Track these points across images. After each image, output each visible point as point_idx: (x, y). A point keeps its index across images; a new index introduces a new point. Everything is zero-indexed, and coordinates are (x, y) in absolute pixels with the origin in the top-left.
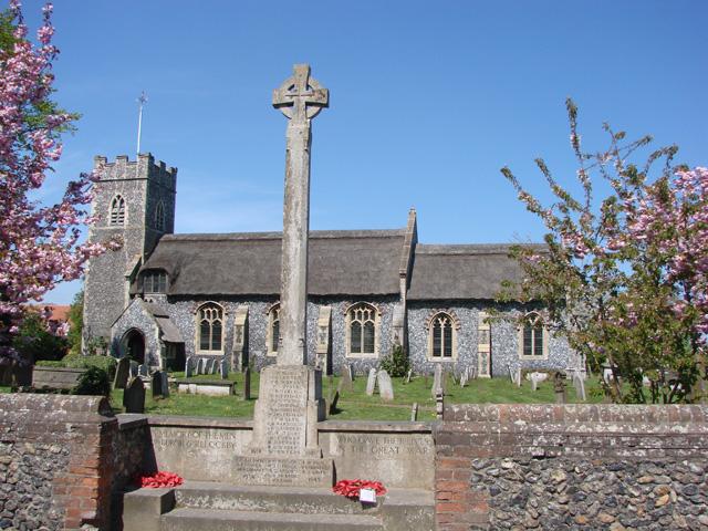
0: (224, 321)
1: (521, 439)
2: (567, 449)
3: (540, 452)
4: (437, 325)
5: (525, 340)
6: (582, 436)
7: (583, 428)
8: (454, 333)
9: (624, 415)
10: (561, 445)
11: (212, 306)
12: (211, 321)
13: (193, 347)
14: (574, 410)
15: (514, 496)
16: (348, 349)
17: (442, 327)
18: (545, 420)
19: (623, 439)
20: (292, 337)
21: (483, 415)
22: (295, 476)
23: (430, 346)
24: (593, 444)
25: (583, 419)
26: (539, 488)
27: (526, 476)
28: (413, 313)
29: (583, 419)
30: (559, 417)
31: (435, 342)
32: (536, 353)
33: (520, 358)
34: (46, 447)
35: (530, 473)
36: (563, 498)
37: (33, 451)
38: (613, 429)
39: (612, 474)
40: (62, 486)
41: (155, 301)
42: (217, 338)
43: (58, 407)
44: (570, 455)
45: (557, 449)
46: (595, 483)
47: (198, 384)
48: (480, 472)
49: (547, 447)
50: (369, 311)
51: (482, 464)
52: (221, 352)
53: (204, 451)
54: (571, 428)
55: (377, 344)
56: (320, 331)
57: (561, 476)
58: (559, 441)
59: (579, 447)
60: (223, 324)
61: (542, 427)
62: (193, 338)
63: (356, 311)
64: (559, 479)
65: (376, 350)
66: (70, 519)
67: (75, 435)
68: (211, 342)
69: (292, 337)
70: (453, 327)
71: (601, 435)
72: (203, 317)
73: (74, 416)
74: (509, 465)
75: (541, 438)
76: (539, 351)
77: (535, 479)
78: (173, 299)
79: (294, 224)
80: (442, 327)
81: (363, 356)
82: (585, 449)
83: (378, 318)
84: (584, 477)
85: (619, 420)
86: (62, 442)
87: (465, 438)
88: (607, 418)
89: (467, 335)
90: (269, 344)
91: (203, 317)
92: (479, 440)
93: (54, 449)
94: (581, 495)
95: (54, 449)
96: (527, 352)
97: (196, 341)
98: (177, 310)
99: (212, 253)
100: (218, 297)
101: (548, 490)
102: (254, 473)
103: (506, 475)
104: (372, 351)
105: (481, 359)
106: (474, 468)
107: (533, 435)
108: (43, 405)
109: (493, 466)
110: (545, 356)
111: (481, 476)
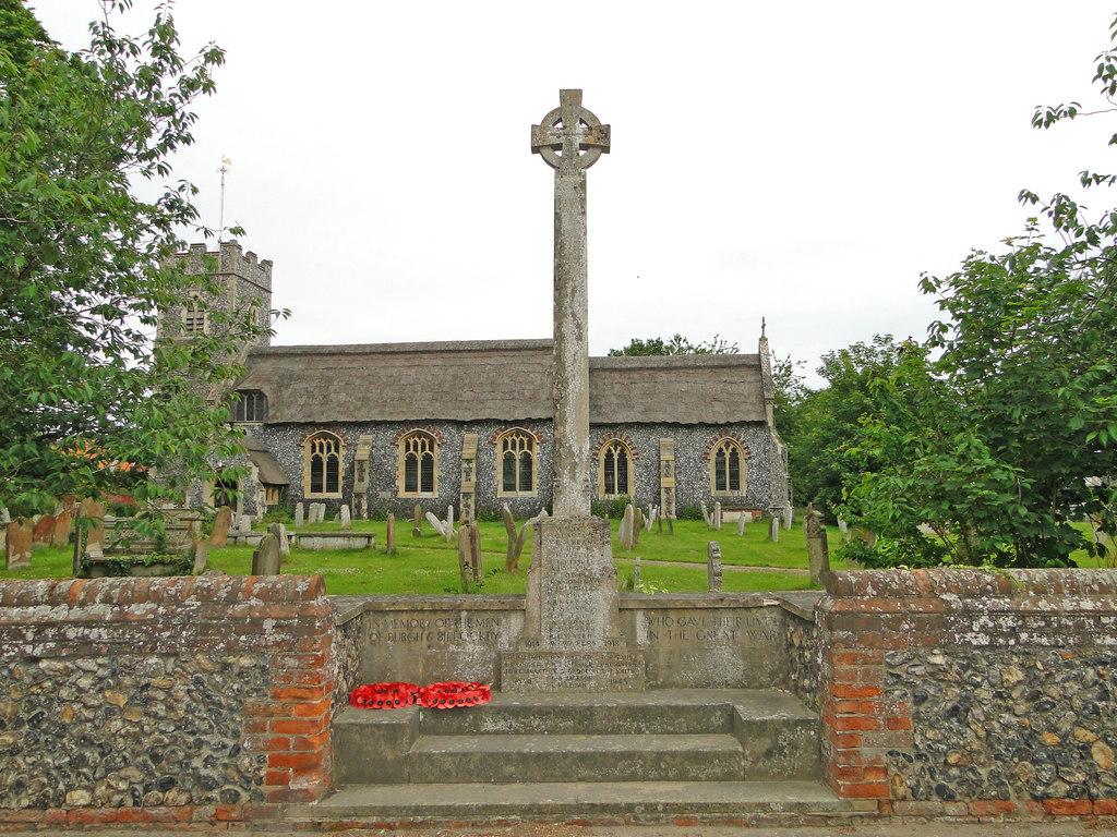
1: (956, 622)
2: (1024, 636)
3: (984, 640)
5: (717, 472)
6: (1044, 616)
7: (1043, 605)
8: (631, 465)
9: (1100, 584)
10: (1013, 629)
11: (326, 436)
13: (302, 490)
14: (1024, 577)
15: (949, 705)
16: (501, 487)
17: (616, 457)
18: (984, 592)
19: (1105, 620)
20: (573, 478)
21: (894, 585)
22: (589, 678)
24: (1060, 626)
25: (1040, 591)
26: (985, 693)
27: (966, 676)
29: (1040, 591)
30: (1007, 590)
31: (607, 475)
34: (231, 659)
35: (970, 672)
36: (1022, 708)
37: (209, 666)
38: (1088, 605)
39: (1091, 672)
40: (257, 719)
41: (248, 432)
42: (333, 478)
43: (248, 594)
44: (1027, 644)
45: (1007, 636)
46: (1067, 685)
47: (324, 536)
48: (897, 671)
49: (993, 633)
50: (525, 440)
51: (898, 660)
52: (338, 495)
53: (452, 648)
54: (1026, 605)
55: (536, 480)
57: (1017, 675)
58: (1010, 623)
59: (1041, 632)
60: (435, 460)
61: (984, 604)
62: (301, 478)
64: (1013, 679)
65: (535, 486)
66: (273, 770)
67: (279, 637)
69: (573, 478)
70: (629, 457)
71: (1073, 614)
73: (276, 610)
74: (939, 660)
75: (984, 619)
76: (735, 486)
77: (979, 680)
79: (570, 318)
80: (616, 457)
82: (1048, 636)
84: (1050, 675)
85: (1092, 591)
86: (254, 650)
87: (873, 621)
88: (1076, 590)
89: (647, 467)
90: (401, 483)
92: (895, 624)
93: (246, 661)
94: (1047, 702)
95: (246, 661)
96: (721, 486)
98: (280, 444)
101: (999, 695)
102: (530, 676)
103: (936, 673)
104: (531, 490)
105: (664, 496)
106: (890, 665)
107: (971, 614)
108: (223, 594)
109: (916, 661)
110: (743, 491)
111: (899, 676)
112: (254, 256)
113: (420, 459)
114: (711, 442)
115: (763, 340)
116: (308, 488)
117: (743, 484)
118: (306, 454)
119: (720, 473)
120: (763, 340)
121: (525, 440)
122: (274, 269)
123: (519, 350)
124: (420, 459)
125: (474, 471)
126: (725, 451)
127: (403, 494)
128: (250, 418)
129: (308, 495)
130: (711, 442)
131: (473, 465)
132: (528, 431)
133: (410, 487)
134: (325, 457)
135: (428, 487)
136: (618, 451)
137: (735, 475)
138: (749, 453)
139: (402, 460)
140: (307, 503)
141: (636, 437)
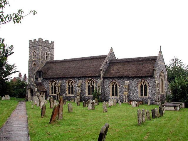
0: (95, 85)
4: (113, 86)
12: (91, 85)
23: (111, 93)
28: (107, 81)
32: (145, 95)
33: (139, 97)
50: (92, 82)
56: (78, 88)
63: (89, 82)
68: (91, 94)
72: (88, 84)
76: (146, 95)
78: (45, 79)
81: (71, 95)
83: (95, 84)
90: (67, 92)
91: (88, 84)
96: (142, 95)
97: (51, 91)
99: (67, 65)
100: (54, 78)
112: (36, 40)
113: (91, 86)
114: (139, 82)
115: (160, 52)
116: (51, 93)
117: (118, 95)
118: (50, 85)
119: (142, 91)
120: (160, 52)
121: (92, 82)
122: (55, 44)
123: (90, 59)
124: (91, 86)
125: (80, 89)
126: (143, 84)
127: (68, 95)
128: (41, 77)
129: (51, 94)
130: (139, 82)
131: (80, 88)
132: (93, 80)
133: (69, 93)
134: (91, 85)
135: (73, 93)
136: (144, 84)
137: (146, 91)
138: (149, 85)
139: (67, 86)
140: (50, 96)
141: (119, 81)
